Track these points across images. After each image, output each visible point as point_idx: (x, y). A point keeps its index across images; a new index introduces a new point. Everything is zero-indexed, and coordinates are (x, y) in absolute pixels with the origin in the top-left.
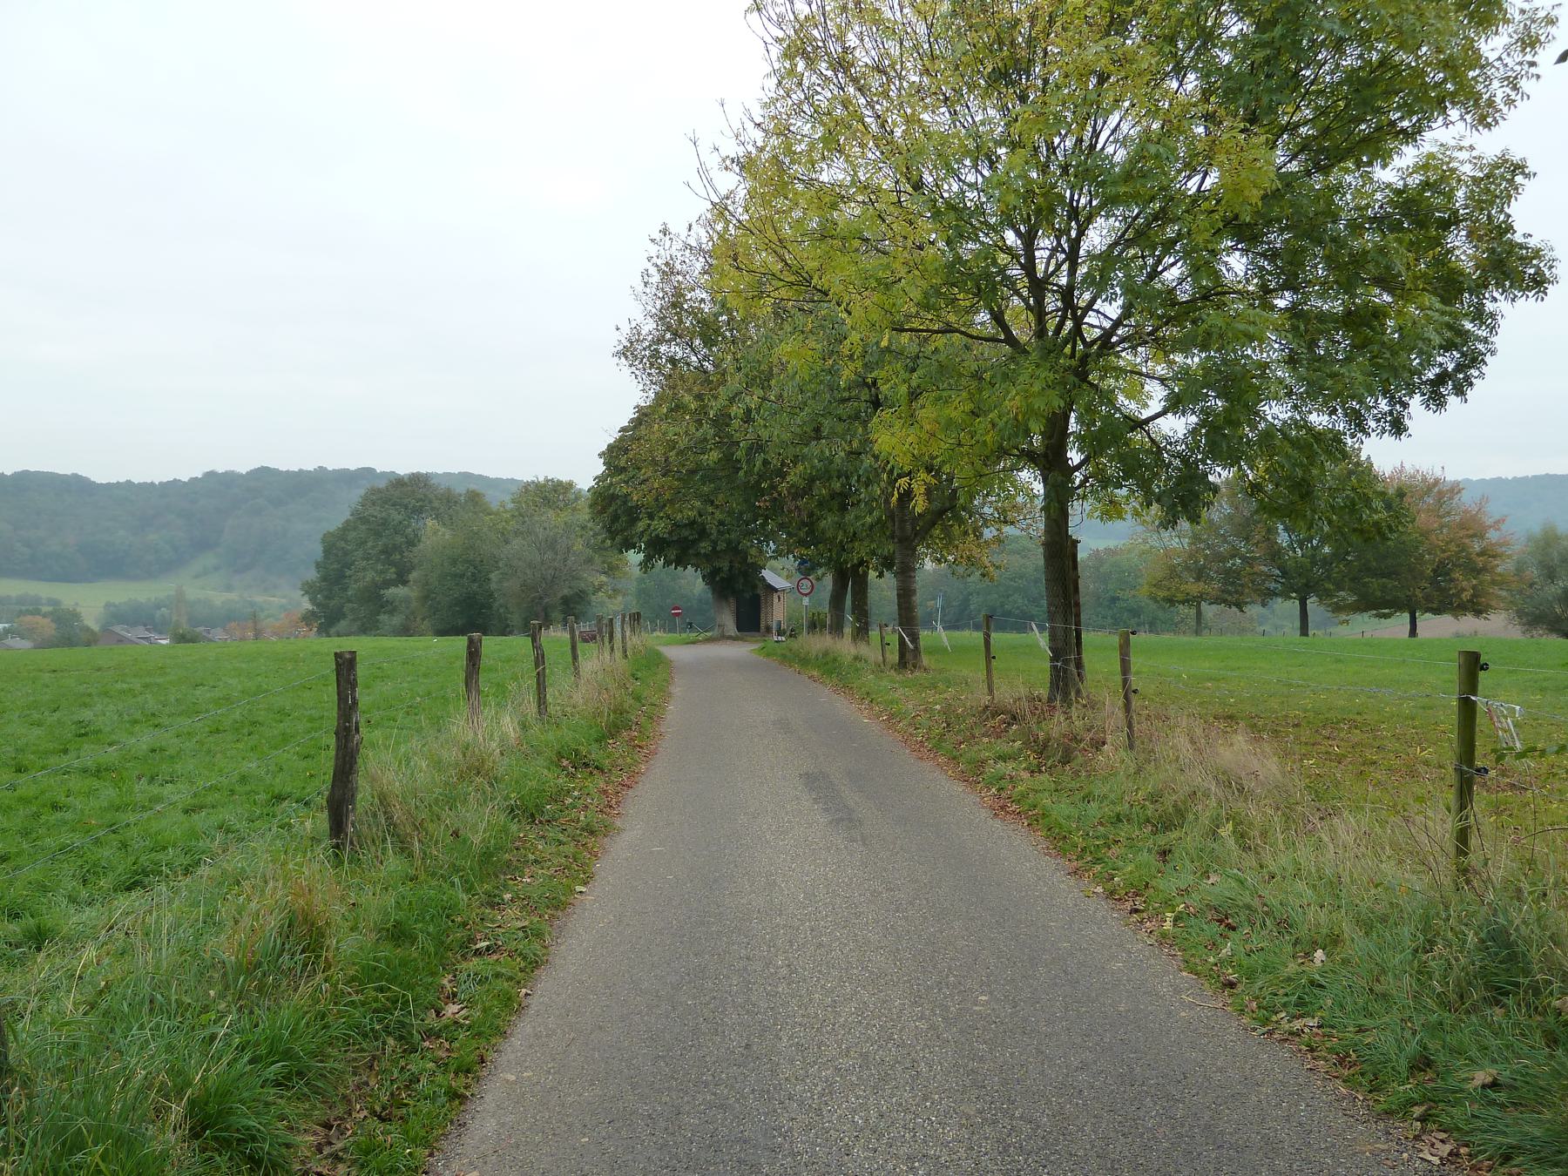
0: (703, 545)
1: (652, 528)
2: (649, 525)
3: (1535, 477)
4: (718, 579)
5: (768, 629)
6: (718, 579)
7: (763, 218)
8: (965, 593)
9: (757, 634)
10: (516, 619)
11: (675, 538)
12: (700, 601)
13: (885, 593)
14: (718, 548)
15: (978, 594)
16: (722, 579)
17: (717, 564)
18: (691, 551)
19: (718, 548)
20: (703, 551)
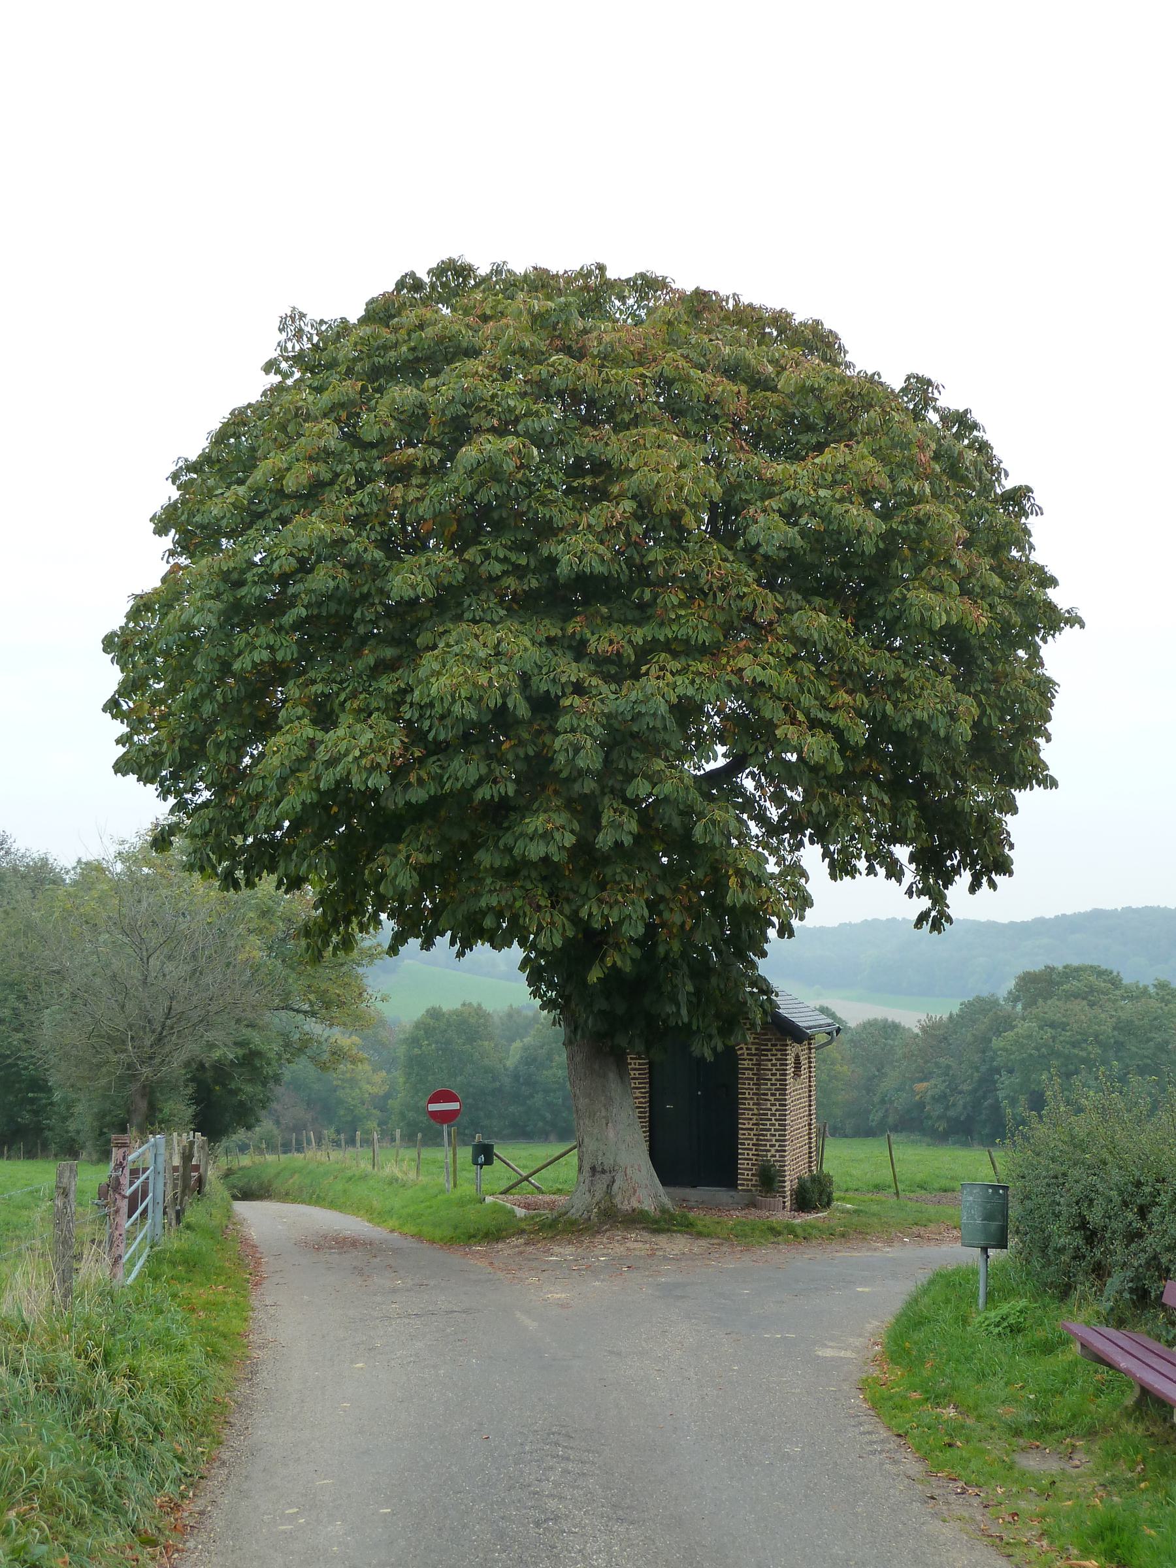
0: (536, 822)
1: (322, 754)
2: (312, 744)
3: (1012, 924)
4: (594, 976)
5: (769, 1179)
6: (594, 976)
7: (40, 1203)
8: (983, 1068)
9: (721, 1195)
10: (82, 1120)
11: (418, 795)
12: (516, 1077)
13: (838, 1067)
14: (604, 840)
15: (1011, 1071)
16: (614, 975)
17: (592, 911)
18: (485, 858)
19: (604, 840)
20: (536, 851)
